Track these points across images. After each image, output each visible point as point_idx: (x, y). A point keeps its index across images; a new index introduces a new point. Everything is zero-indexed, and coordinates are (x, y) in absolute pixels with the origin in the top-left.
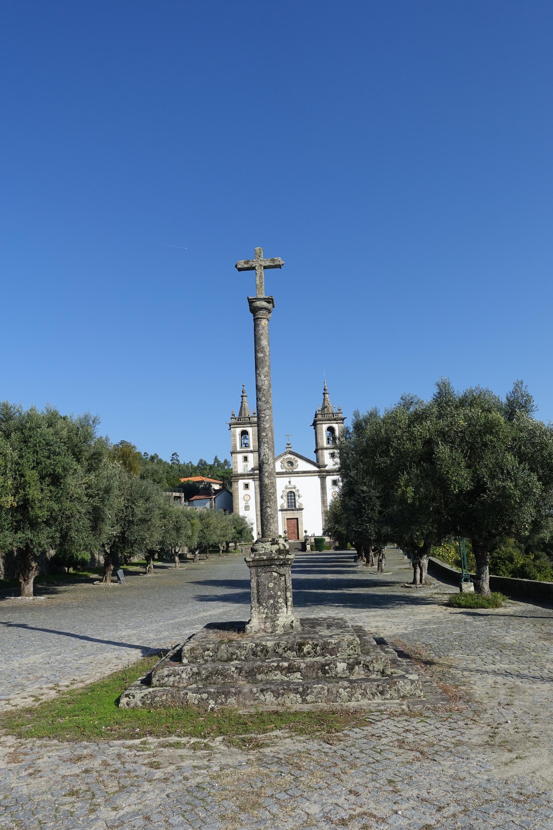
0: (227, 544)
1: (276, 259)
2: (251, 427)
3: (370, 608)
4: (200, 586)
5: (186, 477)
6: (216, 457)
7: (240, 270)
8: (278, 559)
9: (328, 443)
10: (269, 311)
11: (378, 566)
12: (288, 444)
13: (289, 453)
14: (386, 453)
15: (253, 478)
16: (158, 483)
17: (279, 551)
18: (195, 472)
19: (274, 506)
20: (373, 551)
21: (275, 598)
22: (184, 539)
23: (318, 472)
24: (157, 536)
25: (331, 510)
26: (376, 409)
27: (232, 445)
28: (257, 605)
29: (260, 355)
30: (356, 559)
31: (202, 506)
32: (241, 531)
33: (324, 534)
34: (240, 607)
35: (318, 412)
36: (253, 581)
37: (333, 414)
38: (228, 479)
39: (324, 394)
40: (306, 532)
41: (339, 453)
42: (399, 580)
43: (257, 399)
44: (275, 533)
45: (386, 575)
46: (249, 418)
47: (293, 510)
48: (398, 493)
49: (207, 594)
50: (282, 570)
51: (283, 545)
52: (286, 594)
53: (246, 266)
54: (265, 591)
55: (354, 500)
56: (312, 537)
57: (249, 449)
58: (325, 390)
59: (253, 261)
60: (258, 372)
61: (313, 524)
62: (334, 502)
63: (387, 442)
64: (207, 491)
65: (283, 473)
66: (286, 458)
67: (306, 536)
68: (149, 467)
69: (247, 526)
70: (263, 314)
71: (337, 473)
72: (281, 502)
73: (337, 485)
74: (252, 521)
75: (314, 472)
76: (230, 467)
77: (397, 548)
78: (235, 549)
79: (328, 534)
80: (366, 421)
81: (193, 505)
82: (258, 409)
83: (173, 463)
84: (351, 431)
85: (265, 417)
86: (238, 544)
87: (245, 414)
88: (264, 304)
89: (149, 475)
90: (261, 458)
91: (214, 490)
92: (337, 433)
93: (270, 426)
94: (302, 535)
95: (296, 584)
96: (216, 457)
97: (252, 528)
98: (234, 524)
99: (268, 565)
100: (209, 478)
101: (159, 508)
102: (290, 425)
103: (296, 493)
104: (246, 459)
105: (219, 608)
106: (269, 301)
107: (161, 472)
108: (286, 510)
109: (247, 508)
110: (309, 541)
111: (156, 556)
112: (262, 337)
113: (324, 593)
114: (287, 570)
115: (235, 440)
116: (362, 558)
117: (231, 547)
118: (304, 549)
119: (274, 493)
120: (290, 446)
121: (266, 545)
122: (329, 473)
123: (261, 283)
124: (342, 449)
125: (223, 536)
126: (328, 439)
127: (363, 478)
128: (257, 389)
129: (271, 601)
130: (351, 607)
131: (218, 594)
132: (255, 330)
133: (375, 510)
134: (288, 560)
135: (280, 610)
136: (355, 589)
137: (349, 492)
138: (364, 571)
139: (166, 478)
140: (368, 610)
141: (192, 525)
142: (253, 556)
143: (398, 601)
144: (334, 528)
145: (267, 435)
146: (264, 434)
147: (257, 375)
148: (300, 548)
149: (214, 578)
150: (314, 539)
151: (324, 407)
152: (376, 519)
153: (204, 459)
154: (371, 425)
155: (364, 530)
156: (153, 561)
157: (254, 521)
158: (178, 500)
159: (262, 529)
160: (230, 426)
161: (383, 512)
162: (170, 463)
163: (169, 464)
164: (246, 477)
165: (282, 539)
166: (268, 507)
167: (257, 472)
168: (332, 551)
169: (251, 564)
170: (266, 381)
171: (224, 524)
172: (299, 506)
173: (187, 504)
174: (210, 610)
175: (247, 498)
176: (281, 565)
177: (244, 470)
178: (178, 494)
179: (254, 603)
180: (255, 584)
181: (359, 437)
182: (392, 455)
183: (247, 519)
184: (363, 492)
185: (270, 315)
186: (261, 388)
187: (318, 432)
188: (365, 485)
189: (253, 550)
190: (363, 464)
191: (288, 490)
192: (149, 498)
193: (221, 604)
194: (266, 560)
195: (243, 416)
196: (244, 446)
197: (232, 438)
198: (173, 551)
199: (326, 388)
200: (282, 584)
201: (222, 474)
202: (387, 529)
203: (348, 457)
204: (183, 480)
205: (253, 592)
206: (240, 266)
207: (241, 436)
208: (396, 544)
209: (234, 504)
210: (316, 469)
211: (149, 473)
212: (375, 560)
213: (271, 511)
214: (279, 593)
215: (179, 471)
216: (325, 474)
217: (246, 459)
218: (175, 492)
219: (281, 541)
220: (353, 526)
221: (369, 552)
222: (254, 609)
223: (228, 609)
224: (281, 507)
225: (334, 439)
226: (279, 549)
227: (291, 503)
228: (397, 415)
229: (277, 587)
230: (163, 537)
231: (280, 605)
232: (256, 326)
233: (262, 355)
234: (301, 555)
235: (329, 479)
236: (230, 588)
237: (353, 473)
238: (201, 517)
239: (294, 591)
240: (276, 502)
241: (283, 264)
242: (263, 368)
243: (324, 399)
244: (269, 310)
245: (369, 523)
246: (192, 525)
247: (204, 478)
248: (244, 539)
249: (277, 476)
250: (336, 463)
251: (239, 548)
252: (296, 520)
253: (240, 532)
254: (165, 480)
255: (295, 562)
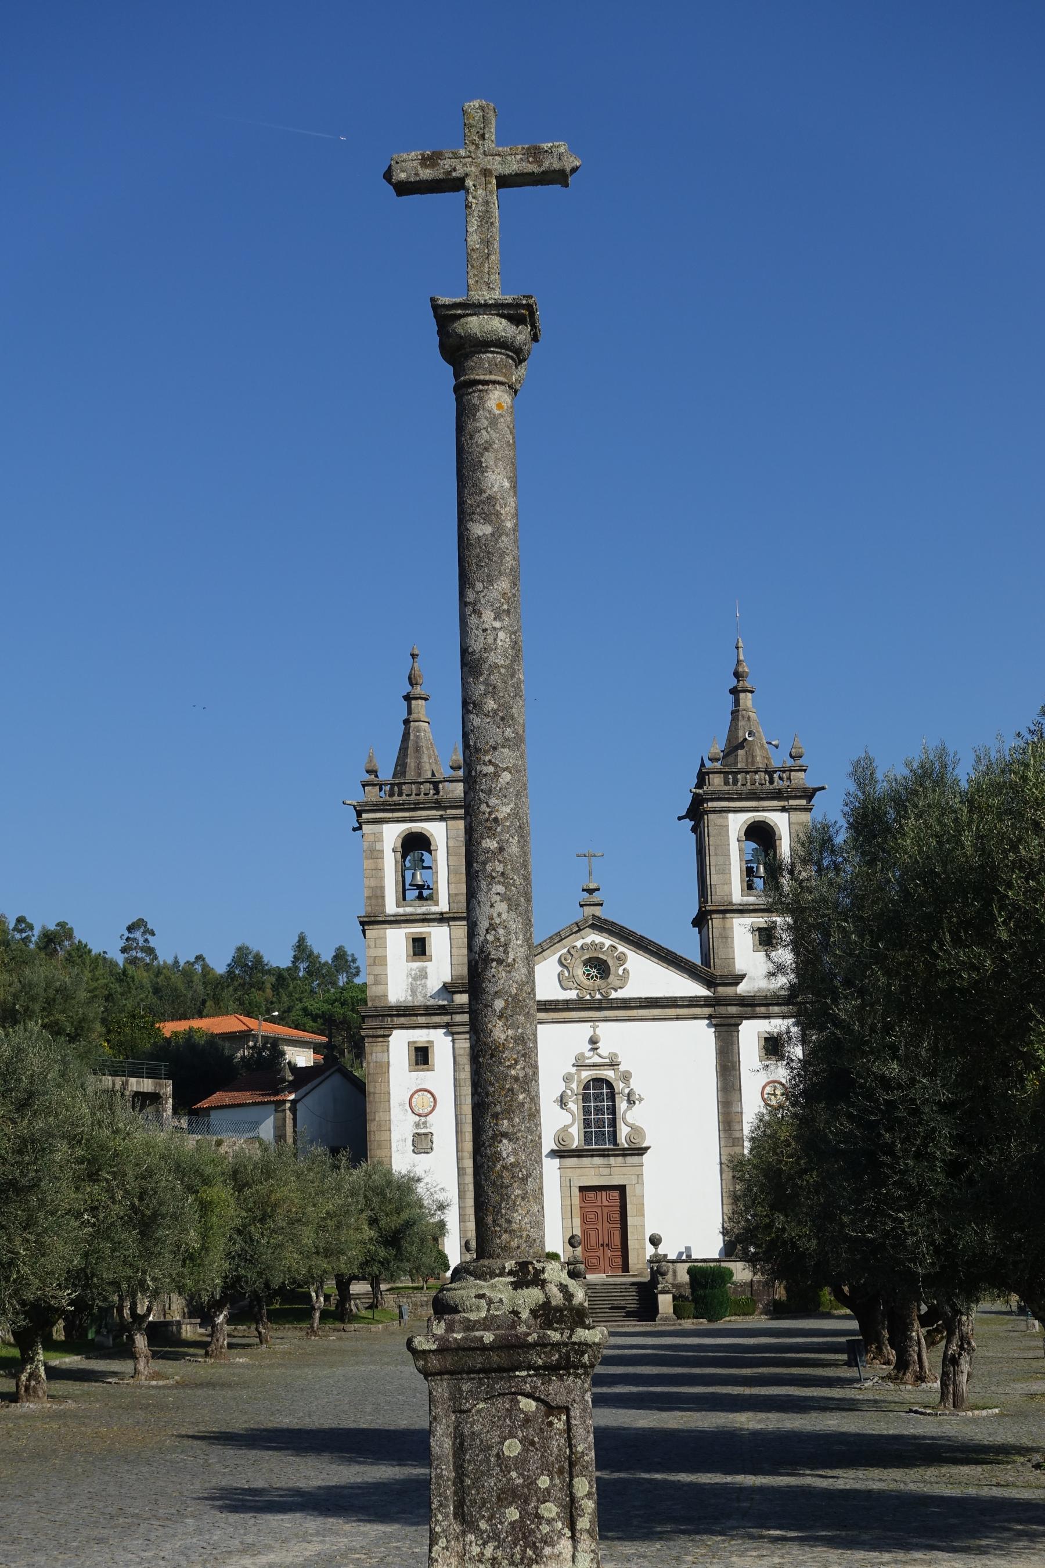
0: (343, 1285)
1: (546, 146)
2: (442, 819)
3: (907, 1547)
4: (230, 1452)
5: (183, 1017)
6: (302, 939)
7: (403, 189)
8: (542, 1344)
9: (750, 887)
10: (518, 355)
11: (944, 1384)
12: (591, 891)
13: (593, 926)
14: (979, 929)
15: (447, 1026)
16: (72, 1039)
17: (546, 1314)
18: (217, 1000)
19: (529, 1130)
20: (924, 1321)
21: (526, 1502)
22: (168, 1264)
23: (706, 1002)
24: (63, 1252)
25: (758, 1156)
26: (942, 753)
27: (367, 893)
28: (457, 1528)
29: (480, 529)
30: (854, 1352)
31: (245, 1134)
32: (398, 1231)
33: (729, 1250)
34: (390, 1537)
35: (709, 765)
36: (439, 1429)
37: (770, 773)
38: (349, 1024)
39: (735, 692)
40: (655, 1241)
41: (790, 928)
42: (1026, 1442)
43: (465, 703)
44: (530, 1242)
45: (974, 1420)
46: (436, 785)
47: (604, 1154)
48: (1023, 1089)
49: (260, 1484)
50: (556, 1389)
51: (563, 1288)
52: (570, 1485)
53: (426, 174)
54: (487, 1473)
55: (850, 1117)
56: (679, 1261)
57: (434, 909)
58: (737, 675)
59: (456, 156)
60: (471, 596)
61: (684, 1211)
62: (768, 1125)
63: (985, 883)
64: (264, 1073)
65: (566, 1006)
66: (579, 944)
67: (658, 1260)
68: (39, 973)
69: (423, 1216)
70: (494, 367)
71: (785, 1009)
72: (557, 1120)
73: (781, 1058)
74: (441, 1197)
75: (692, 1002)
76: (358, 981)
77: (1021, 1311)
78: (372, 1307)
79: (745, 1251)
80: (902, 800)
81: (208, 1129)
82: (466, 746)
83: (133, 961)
84: (840, 838)
85: (496, 775)
86: (383, 1287)
87: (419, 767)
88: (499, 326)
89: (37, 1007)
90: (479, 940)
91: (293, 1068)
92: (785, 848)
93: (515, 814)
94: (641, 1254)
95: (611, 1446)
96: (302, 939)
97: (442, 1225)
98: (368, 1204)
99: (500, 1369)
100: (273, 1020)
101: (74, 1140)
102: (597, 809)
103: (619, 1086)
104: (419, 947)
105: (305, 1538)
106: (519, 313)
107: (83, 995)
108: (578, 1153)
109: (422, 1142)
110: (669, 1277)
111: (58, 1332)
112: (488, 459)
113: (665, 1481)
114: (576, 1391)
115: (379, 870)
116: (879, 1349)
117: (358, 1296)
118: (647, 1309)
119: (529, 1081)
120: (596, 897)
121: (493, 1287)
122: (753, 1006)
123: (487, 243)
124: (803, 910)
125: (328, 1253)
126: (750, 872)
127: (888, 1029)
128: (464, 664)
129: (513, 1514)
130: (832, 1542)
131: (302, 1484)
132: (460, 429)
133: (932, 1157)
134: (583, 1347)
135: (547, 1551)
136: (851, 1473)
137: (826, 1085)
138: (886, 1401)
139: (104, 1021)
140: (901, 1555)
141: (205, 1207)
142: (439, 1329)
143: (1020, 1522)
144: (769, 1226)
145: (501, 849)
146: (493, 845)
147: (467, 608)
148: (632, 1305)
149: (286, 1421)
150: (690, 1271)
151: (734, 746)
152: (938, 1192)
153: (255, 947)
154: (918, 817)
155: (886, 1235)
156: (46, 1349)
157: (451, 1194)
158: (150, 1110)
159: (480, 1222)
160: (359, 814)
161: (966, 1165)
162: (120, 959)
163: (113, 964)
164: (422, 1020)
165: (556, 1265)
166: (505, 1135)
167: (462, 999)
168: (758, 1321)
169: (434, 1363)
170: (501, 635)
171: (330, 1207)
172: (629, 1139)
173: (184, 1123)
174: (270, 1548)
175: (422, 1104)
176: (553, 1369)
177: (414, 992)
178: (147, 1085)
179: (444, 1520)
180: (448, 1443)
181: (871, 863)
182: (1004, 936)
183: (421, 1189)
184: (885, 1083)
185: (522, 370)
186: (481, 661)
187: (712, 841)
188: (895, 1057)
189: (442, 1308)
190: (888, 973)
191: (586, 1075)
192: (31, 1094)
193: (312, 1523)
194: (491, 1347)
195: (411, 775)
196: (412, 894)
197: (368, 864)
198: (126, 1313)
199: (745, 668)
200: (557, 1443)
201: (326, 1007)
202: (978, 1236)
203: (825, 945)
204: (169, 1028)
205: (439, 1477)
206: (403, 176)
207: (404, 857)
208: (1014, 1298)
209: (371, 1127)
210: (698, 990)
211: (33, 999)
212: (932, 1359)
213: (515, 1152)
214: (544, 1482)
215: (156, 990)
216: (733, 1010)
217: (419, 947)
218: (138, 1074)
219: (554, 1273)
220: (845, 1219)
221: (906, 1328)
222: (442, 1542)
223: (342, 1542)
224: (559, 1140)
225: (774, 870)
226: (547, 1304)
227: (600, 1124)
228: (1024, 779)
229: (535, 1457)
230: (86, 1255)
231: (545, 1529)
232: (465, 413)
233: (488, 530)
234: (636, 1337)
235: (751, 1033)
236: (351, 1461)
237: (844, 1009)
238: (238, 1178)
239: (604, 1475)
240: (534, 1115)
241: (574, 170)
242: (490, 581)
243: (735, 714)
244: (518, 351)
245: (910, 1207)
246: (205, 1207)
247: (252, 1023)
248: (408, 1266)
249: (541, 1015)
250: (780, 968)
251: (390, 1301)
252: (615, 1194)
253: (393, 1240)
254: (99, 1028)
255: (607, 1361)
